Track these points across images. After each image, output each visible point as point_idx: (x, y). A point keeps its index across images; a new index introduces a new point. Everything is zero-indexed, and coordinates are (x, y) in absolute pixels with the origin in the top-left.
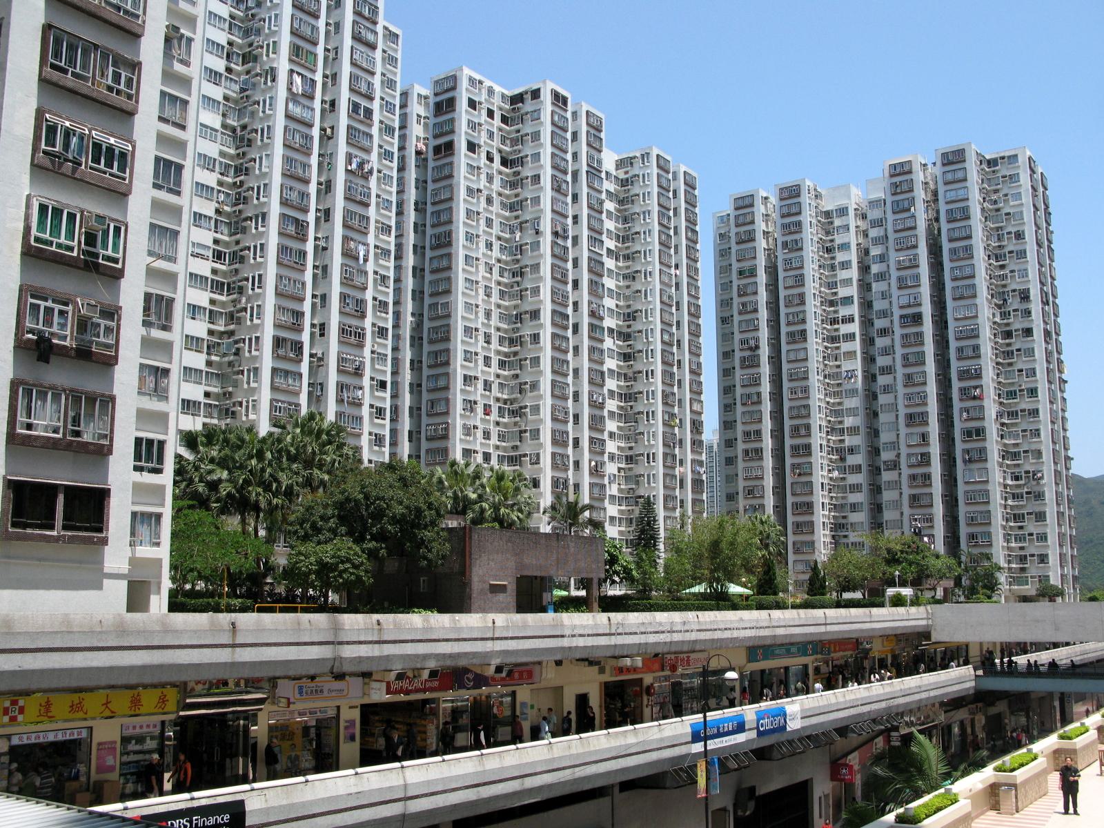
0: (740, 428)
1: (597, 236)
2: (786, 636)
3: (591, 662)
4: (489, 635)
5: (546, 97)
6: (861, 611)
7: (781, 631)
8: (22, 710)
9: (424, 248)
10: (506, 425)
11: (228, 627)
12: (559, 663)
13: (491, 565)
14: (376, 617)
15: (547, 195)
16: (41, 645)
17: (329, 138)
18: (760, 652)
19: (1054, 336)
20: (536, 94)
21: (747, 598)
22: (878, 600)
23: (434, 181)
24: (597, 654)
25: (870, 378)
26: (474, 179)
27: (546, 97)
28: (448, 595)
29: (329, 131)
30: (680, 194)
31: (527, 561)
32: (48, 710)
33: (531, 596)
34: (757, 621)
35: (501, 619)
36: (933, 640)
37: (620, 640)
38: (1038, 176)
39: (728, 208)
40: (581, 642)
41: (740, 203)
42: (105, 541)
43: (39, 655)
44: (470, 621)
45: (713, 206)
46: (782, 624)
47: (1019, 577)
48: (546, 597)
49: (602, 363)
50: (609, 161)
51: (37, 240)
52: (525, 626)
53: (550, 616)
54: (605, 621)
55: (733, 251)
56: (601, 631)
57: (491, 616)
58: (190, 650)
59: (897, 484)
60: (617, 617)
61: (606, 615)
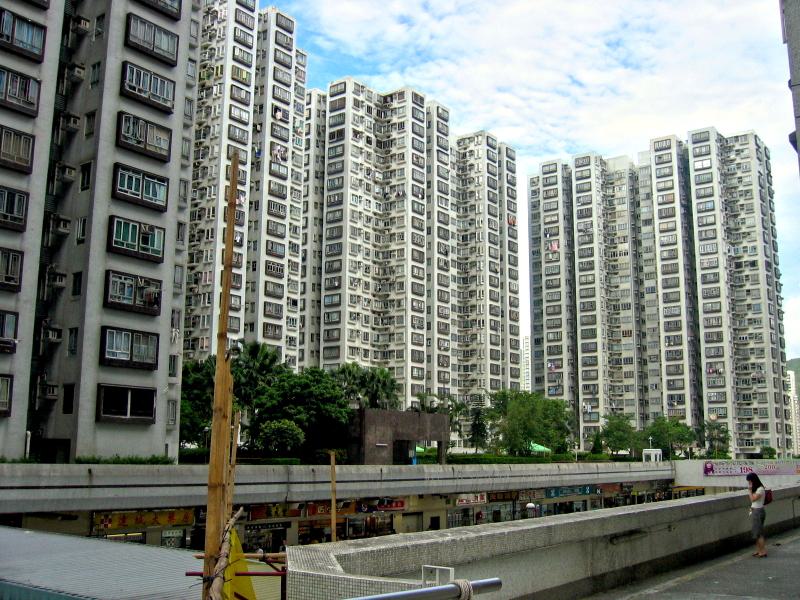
0: (546, 345)
1: (443, 196)
2: (570, 481)
3: (441, 496)
4: (379, 478)
5: (409, 98)
6: (623, 464)
7: (567, 478)
8: (110, 521)
9: (322, 204)
10: (379, 330)
11: (86, 473)
12: (421, 497)
13: (378, 436)
14: (312, 467)
15: (409, 167)
16: (128, 483)
17: (259, 132)
18: (553, 492)
19: (774, 266)
20: (401, 94)
21: (547, 454)
22: (598, 456)
23: (329, 158)
24: (444, 491)
25: (639, 295)
26: (357, 157)
27: (409, 98)
28: (354, 453)
29: (258, 127)
30: (503, 159)
31: (400, 430)
32: (124, 522)
33: (401, 453)
34: (550, 470)
35: (385, 468)
36: (676, 485)
37: (459, 482)
38: (762, 150)
39: (537, 172)
40: (434, 483)
41: (547, 169)
42: (153, 422)
43: (140, 489)
44: (369, 470)
45: (527, 169)
46: (567, 472)
47: (745, 440)
48: (411, 454)
49: (447, 271)
50: (452, 141)
51: (116, 242)
52: (193, 474)
53: (414, 466)
54: (450, 469)
55: (542, 204)
56: (448, 477)
57: (379, 467)
58: (142, 488)
59: (658, 373)
60: (458, 467)
61: (451, 466)
